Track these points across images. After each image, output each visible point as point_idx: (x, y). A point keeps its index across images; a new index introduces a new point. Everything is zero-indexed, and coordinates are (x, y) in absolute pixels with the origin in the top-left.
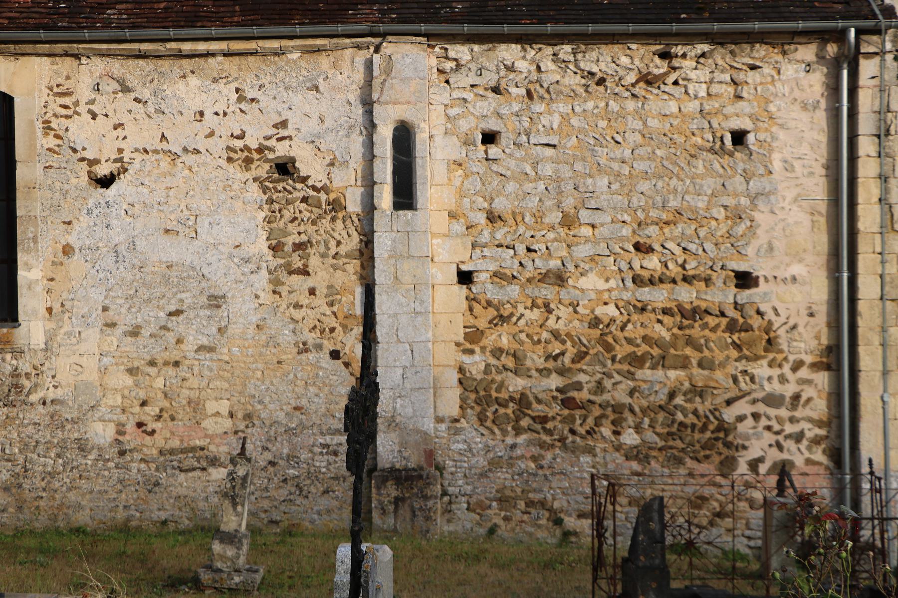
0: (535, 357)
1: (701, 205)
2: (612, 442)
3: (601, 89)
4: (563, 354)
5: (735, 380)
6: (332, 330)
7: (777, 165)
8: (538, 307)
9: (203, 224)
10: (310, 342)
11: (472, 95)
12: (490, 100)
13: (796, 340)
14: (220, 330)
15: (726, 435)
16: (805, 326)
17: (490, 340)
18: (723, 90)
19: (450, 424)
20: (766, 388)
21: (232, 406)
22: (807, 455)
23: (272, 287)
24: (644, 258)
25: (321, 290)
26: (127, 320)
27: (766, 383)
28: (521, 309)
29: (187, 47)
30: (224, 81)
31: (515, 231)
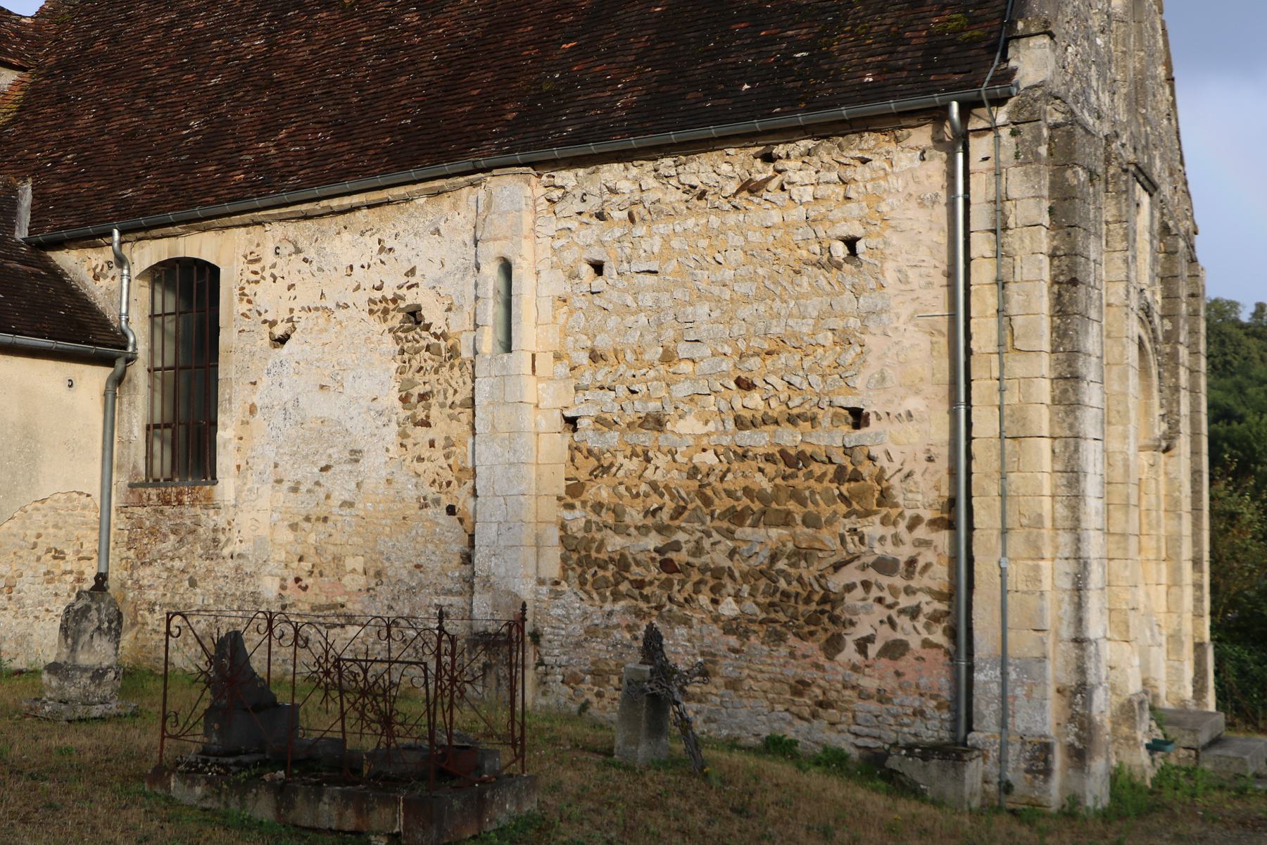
0: (634, 513)
1: (805, 329)
2: (711, 612)
3: (702, 203)
4: (660, 508)
5: (842, 538)
6: (449, 484)
7: (890, 277)
8: (638, 456)
9: (349, 377)
10: (430, 497)
11: (576, 224)
12: (594, 227)
13: (911, 491)
14: (358, 484)
15: (833, 608)
16: (923, 474)
17: (590, 494)
18: (830, 192)
19: (552, 587)
20: (876, 551)
21: (365, 563)
22: (925, 634)
23: (400, 440)
24: (745, 396)
25: (440, 443)
26: (290, 476)
27: (876, 544)
28: (620, 459)
29: (335, 203)
30: (369, 233)
31: (616, 371)
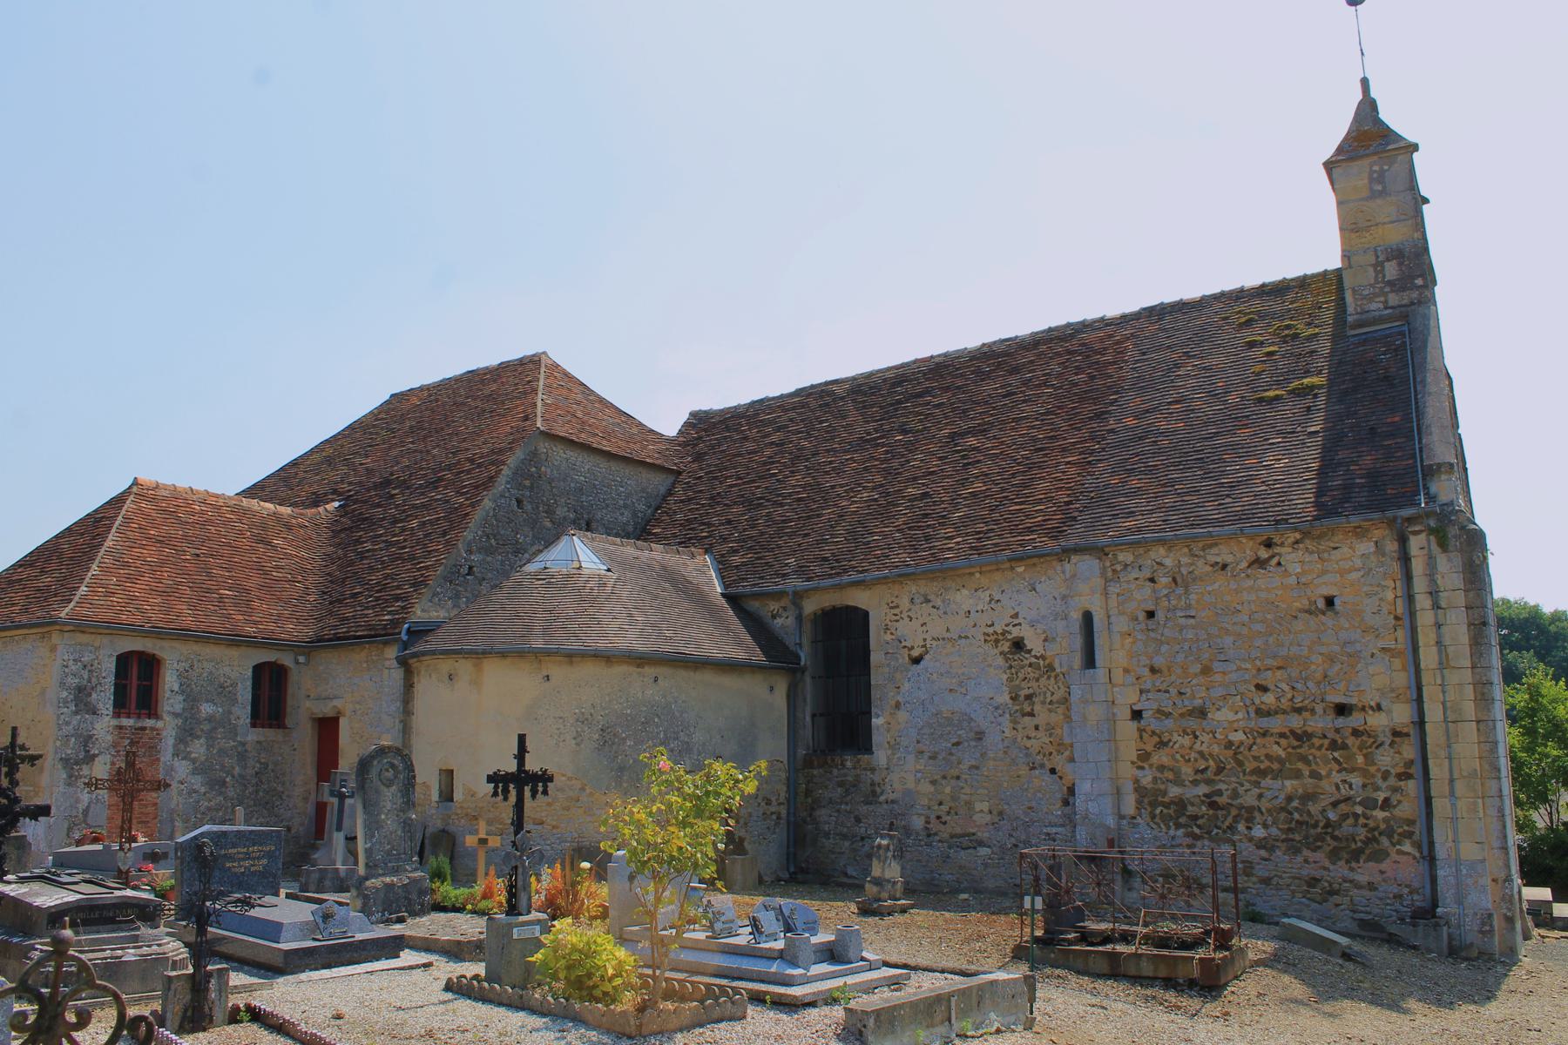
23: (1012, 725)
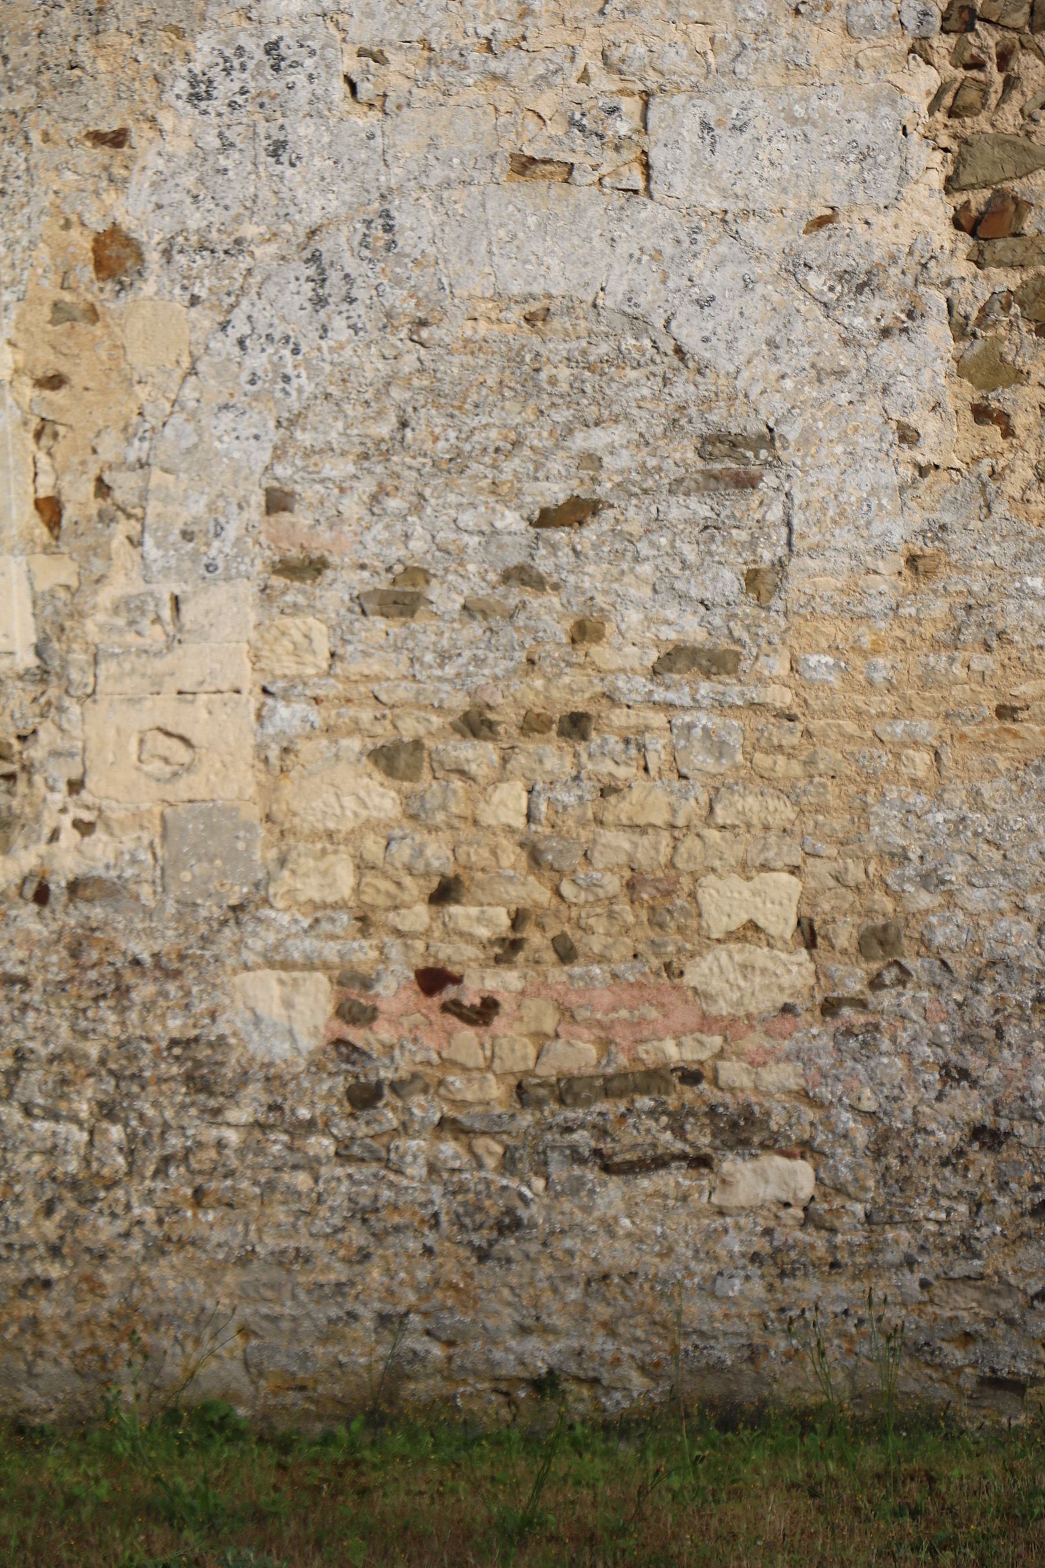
21: (809, 898)
23: (970, 393)
